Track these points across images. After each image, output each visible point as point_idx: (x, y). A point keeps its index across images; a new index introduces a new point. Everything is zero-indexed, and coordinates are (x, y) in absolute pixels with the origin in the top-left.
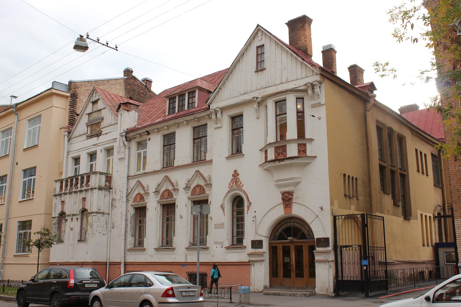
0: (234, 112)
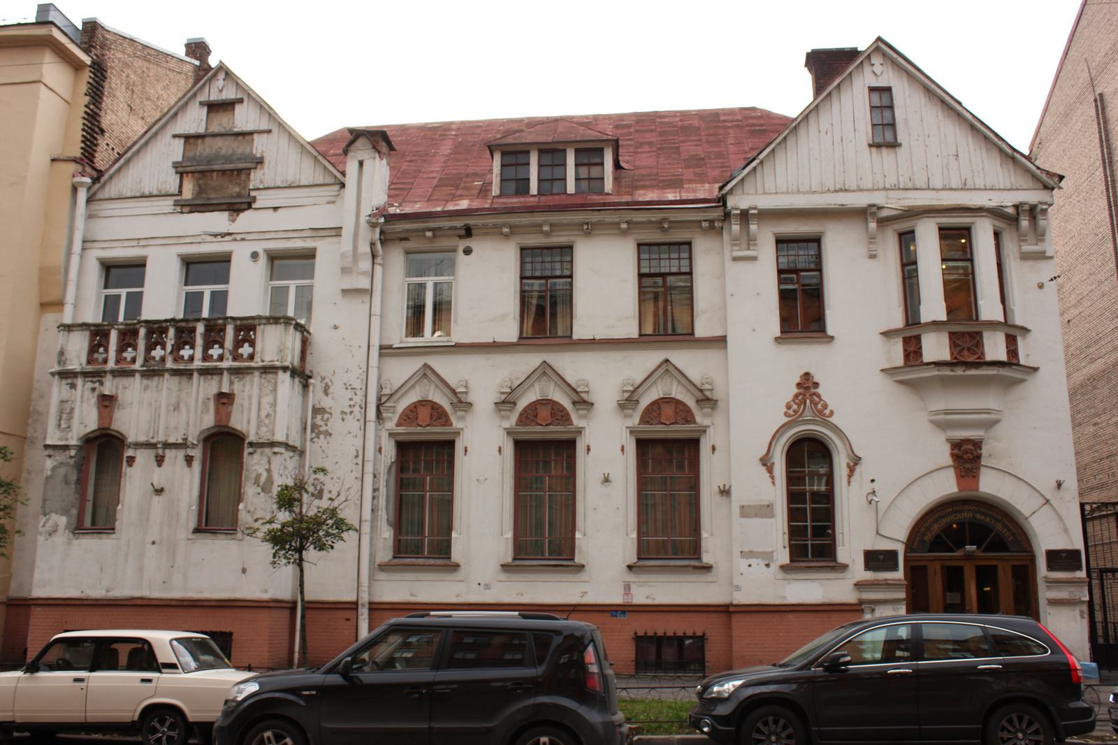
0: (904, 226)
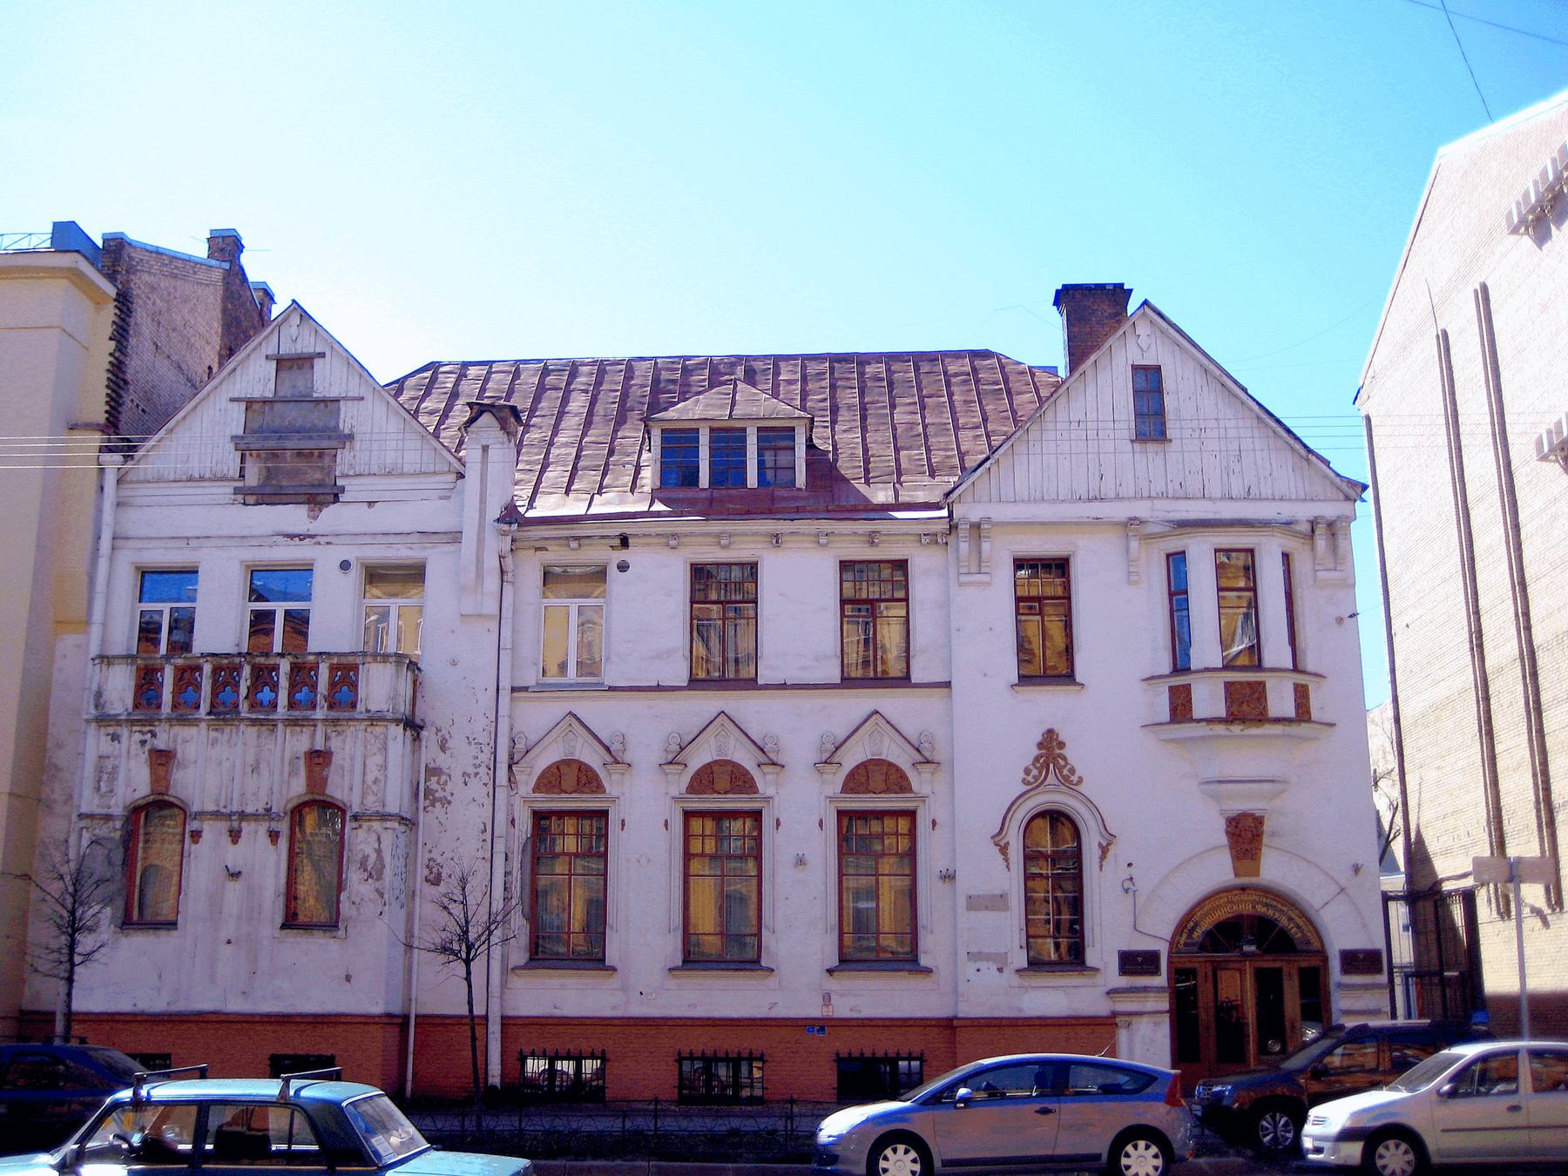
0: (1174, 545)
